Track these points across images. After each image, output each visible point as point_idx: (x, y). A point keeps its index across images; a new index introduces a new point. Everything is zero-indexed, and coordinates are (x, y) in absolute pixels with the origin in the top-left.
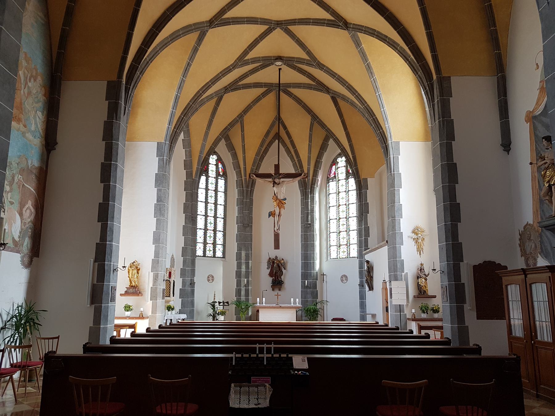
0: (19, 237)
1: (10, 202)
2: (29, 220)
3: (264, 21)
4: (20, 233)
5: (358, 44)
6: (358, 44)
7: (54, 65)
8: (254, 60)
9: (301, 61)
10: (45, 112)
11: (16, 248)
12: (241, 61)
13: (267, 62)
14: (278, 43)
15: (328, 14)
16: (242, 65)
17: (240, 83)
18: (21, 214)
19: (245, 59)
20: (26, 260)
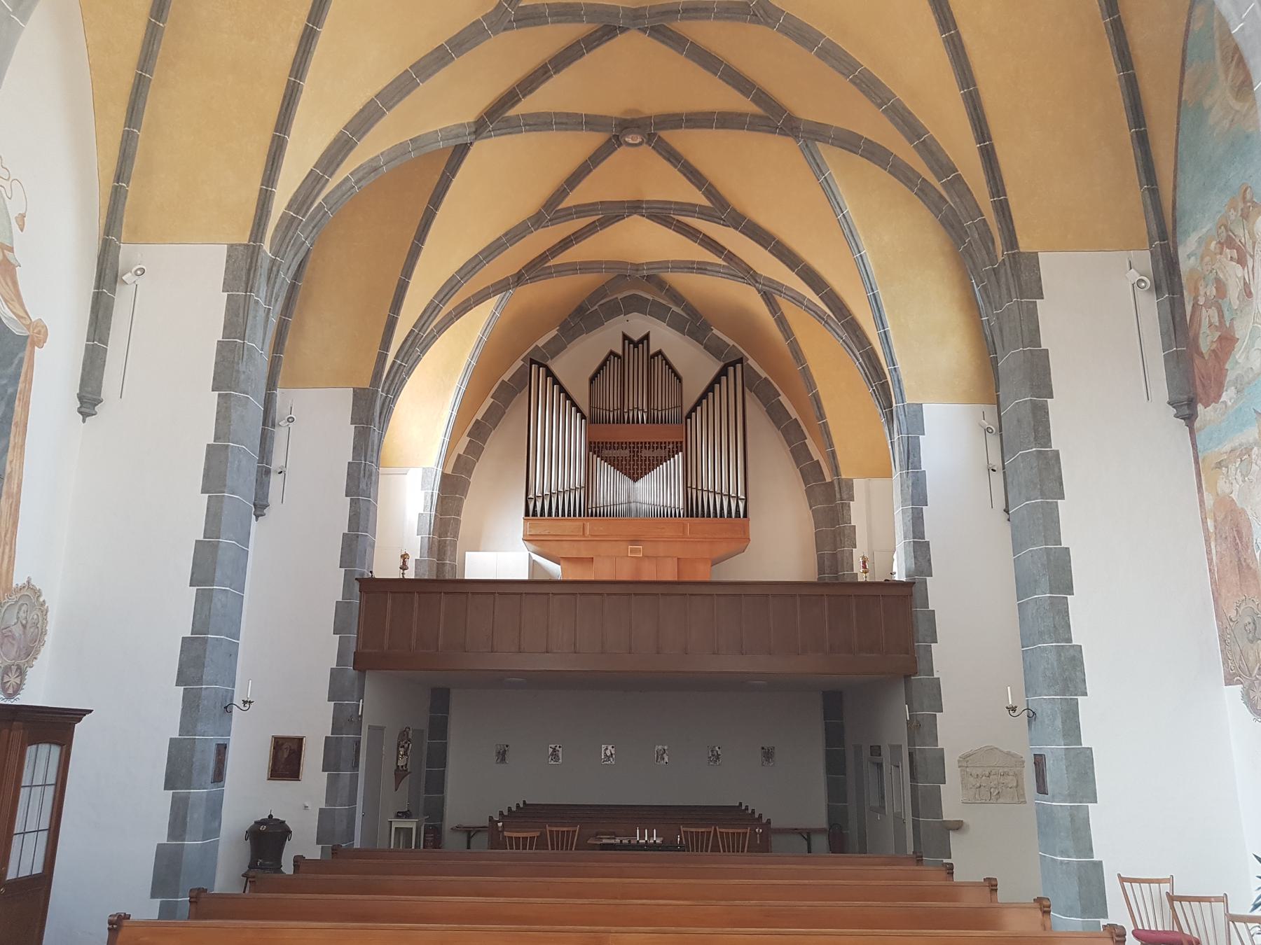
3: (591, 123)
5: (818, 168)
6: (818, 168)
7: (344, 171)
8: (581, 211)
9: (690, 209)
12: (550, 212)
13: (611, 213)
14: (639, 173)
15: (283, 209)
16: (553, 221)
17: (552, 262)
19: (560, 207)
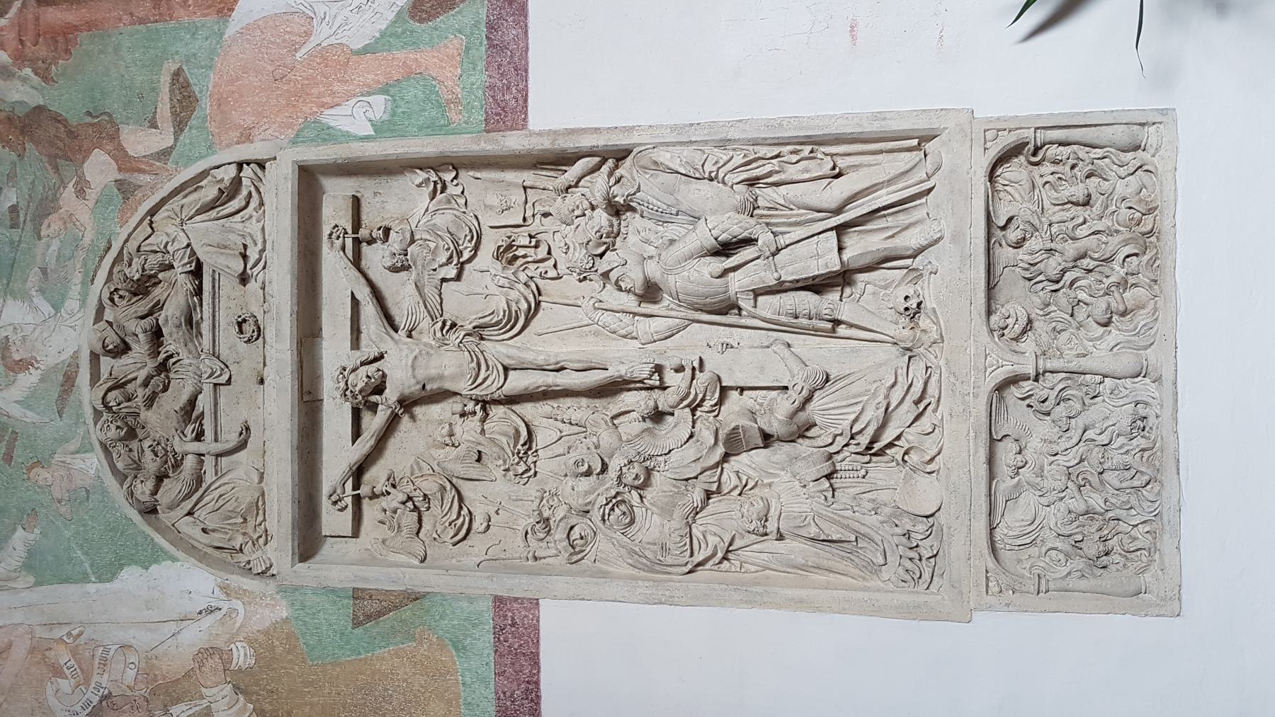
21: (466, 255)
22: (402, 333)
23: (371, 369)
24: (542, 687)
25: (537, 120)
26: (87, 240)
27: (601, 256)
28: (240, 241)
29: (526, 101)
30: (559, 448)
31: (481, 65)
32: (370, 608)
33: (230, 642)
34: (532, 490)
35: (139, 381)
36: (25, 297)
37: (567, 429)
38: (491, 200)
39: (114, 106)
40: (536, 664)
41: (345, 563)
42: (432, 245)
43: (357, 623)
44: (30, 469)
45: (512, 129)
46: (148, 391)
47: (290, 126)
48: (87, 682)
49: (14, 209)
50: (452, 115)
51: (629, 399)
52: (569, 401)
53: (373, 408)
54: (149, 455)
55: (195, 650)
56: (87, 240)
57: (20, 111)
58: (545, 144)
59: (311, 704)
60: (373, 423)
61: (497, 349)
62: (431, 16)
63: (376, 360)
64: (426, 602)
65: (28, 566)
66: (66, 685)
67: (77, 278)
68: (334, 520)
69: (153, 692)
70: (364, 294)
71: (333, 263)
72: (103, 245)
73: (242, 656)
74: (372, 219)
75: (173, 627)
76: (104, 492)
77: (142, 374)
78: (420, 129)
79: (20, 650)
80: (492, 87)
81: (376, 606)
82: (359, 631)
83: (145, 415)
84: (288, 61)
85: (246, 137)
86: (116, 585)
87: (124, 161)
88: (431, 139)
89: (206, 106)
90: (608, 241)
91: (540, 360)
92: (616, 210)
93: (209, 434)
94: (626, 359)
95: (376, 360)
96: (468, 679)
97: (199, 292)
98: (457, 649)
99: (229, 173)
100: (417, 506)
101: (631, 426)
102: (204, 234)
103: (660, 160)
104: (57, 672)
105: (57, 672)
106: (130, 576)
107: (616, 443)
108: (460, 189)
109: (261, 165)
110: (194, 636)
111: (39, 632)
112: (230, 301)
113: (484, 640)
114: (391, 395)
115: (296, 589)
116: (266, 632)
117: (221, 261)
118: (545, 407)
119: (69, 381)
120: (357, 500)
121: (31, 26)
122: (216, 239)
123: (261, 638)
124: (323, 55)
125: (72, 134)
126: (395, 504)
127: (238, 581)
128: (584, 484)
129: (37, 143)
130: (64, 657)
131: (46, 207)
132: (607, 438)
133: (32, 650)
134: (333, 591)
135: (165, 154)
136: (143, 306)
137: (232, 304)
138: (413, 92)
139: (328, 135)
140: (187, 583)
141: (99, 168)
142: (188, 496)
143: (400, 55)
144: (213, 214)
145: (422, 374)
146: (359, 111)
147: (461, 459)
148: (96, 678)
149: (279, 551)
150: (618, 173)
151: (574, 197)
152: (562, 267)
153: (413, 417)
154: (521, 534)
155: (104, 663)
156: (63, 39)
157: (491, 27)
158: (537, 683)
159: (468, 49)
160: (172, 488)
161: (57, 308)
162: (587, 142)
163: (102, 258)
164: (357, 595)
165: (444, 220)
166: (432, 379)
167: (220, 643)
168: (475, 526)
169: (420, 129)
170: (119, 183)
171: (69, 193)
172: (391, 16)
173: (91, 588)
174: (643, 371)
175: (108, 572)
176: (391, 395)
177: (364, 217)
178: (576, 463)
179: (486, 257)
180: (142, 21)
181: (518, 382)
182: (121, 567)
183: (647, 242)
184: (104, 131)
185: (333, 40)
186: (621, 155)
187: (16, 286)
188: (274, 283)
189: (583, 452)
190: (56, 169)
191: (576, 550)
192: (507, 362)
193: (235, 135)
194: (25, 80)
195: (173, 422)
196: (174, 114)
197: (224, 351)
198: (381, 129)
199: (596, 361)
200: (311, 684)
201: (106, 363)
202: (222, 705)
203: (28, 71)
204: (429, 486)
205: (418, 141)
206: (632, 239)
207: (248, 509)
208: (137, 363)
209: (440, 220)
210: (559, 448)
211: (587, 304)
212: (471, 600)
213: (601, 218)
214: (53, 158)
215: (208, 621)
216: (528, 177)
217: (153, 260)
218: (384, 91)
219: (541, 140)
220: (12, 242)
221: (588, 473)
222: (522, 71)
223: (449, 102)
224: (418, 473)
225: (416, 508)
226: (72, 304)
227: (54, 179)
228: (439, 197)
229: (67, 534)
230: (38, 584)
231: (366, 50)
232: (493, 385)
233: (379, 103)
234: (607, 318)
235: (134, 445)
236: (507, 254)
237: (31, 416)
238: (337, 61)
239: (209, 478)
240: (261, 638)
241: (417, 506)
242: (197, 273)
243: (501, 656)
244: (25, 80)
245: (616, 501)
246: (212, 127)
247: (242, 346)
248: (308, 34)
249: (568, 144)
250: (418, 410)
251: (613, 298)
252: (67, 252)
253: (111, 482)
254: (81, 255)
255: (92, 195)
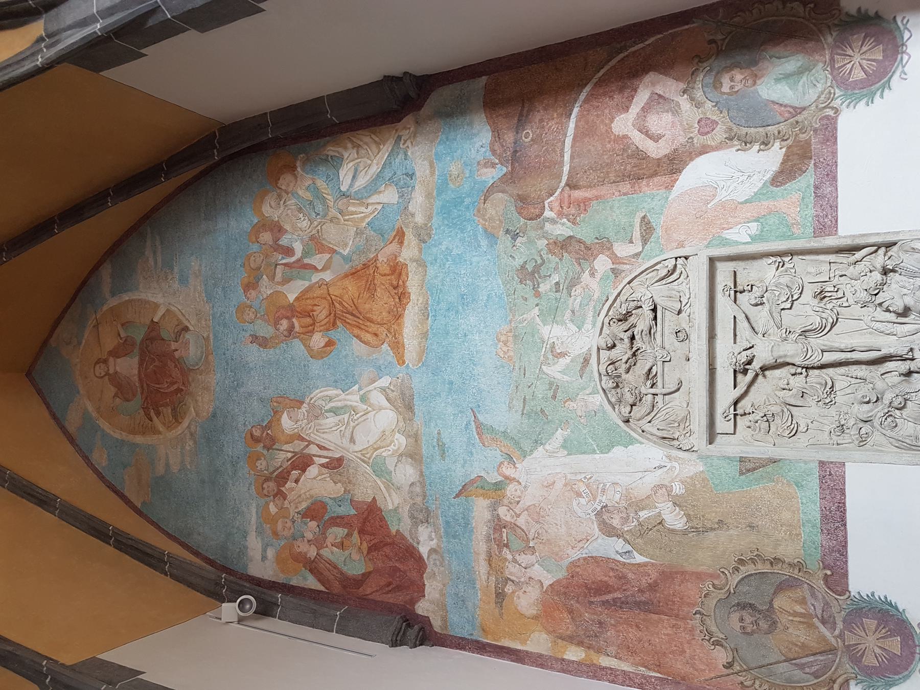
0: (766, 143)
1: (645, 241)
2: (684, 103)
4: (746, 142)
10: (331, 150)
11: (808, 153)
18: (673, 164)
20: (859, 59)
21: (795, 297)
22: (760, 335)
23: (749, 352)
24: (847, 505)
25: (841, 232)
26: (596, 297)
27: (876, 295)
28: (678, 295)
29: (837, 221)
30: (849, 391)
31: (811, 206)
32: (748, 466)
33: (672, 481)
34: (833, 411)
35: (624, 361)
36: (563, 323)
37: (854, 381)
38: (810, 271)
39: (611, 234)
40: (843, 492)
41: (732, 446)
42: (777, 293)
43: (741, 473)
44: (565, 403)
45: (829, 235)
46: (628, 365)
47: (705, 239)
48: (595, 499)
49: (557, 284)
50: (795, 230)
51: (890, 365)
52: (855, 367)
53: (745, 372)
54: (628, 394)
55: (652, 486)
56: (596, 297)
57: (560, 239)
58: (849, 242)
59: (716, 512)
60: (744, 381)
61: (816, 342)
62: (782, 184)
63: (750, 348)
64: (781, 464)
65: (564, 447)
66: (583, 501)
67: (591, 314)
68: (722, 425)
69: (630, 505)
70: (741, 318)
71: (723, 303)
72: (605, 298)
73: (678, 489)
74: (742, 283)
75: (640, 475)
76: (604, 412)
77: (625, 358)
78: (777, 237)
79: (559, 485)
80: (817, 216)
81: (752, 465)
82: (743, 477)
83: (624, 376)
84: (704, 208)
85: (681, 245)
86: (610, 455)
87: (615, 259)
88: (781, 243)
89: (659, 232)
90: (880, 288)
91: (842, 346)
92: (885, 272)
93: (659, 384)
94: (890, 346)
95: (750, 348)
96: (804, 501)
97: (655, 318)
98: (798, 486)
99: (671, 264)
100: (768, 419)
101: (894, 379)
102: (659, 293)
103: (916, 247)
104: (579, 495)
105: (579, 495)
106: (618, 451)
107: (886, 387)
108: (792, 266)
109: (686, 258)
110: (652, 479)
111: (569, 476)
112: (668, 322)
113: (814, 483)
114: (756, 365)
115: (708, 457)
116: (691, 478)
117: (669, 304)
118: (842, 370)
119: (586, 361)
120: (735, 415)
121: (566, 200)
122: (666, 293)
123: (688, 480)
124: (723, 205)
125: (588, 248)
126: (758, 418)
127: (675, 453)
128: (866, 407)
129: (569, 253)
130: (582, 488)
131: (573, 283)
132: (880, 385)
133: (565, 485)
134: (729, 458)
135: (637, 255)
136: (625, 326)
137: (672, 324)
138: (773, 220)
139: (725, 242)
140: (648, 454)
141: (602, 263)
142: (649, 414)
143: (765, 203)
144: (664, 282)
145: (776, 354)
146: (743, 231)
147: (794, 396)
148: (599, 498)
149: (698, 438)
150: (889, 254)
151: (861, 267)
152: (851, 301)
153: (764, 376)
154: (827, 433)
155: (603, 491)
156: (583, 205)
157: (816, 187)
158: (844, 503)
159: (803, 198)
160: (638, 411)
161: (580, 328)
162: (872, 240)
163: (604, 305)
164: (742, 460)
165: (785, 280)
166: (780, 357)
167: (666, 483)
168: (800, 429)
169: (777, 237)
170: (613, 270)
171: (586, 275)
172: (760, 185)
173: (597, 456)
174: (902, 351)
175: (607, 448)
176: (756, 365)
177: (738, 280)
178: (863, 397)
179: (808, 296)
180: (625, 194)
181: (829, 358)
182: (613, 447)
183: (904, 287)
184: (605, 245)
185: (728, 198)
186: (889, 245)
187: (558, 319)
188: (696, 314)
189: (864, 391)
190: (580, 264)
191: (862, 441)
192: (823, 348)
193: (675, 245)
194: (563, 224)
195: (643, 378)
196: (642, 236)
197: (667, 346)
198: (754, 239)
199: (876, 346)
200: (716, 502)
201: (604, 354)
202: (667, 511)
203: (565, 220)
204: (776, 409)
205: (776, 243)
206: (894, 286)
207: (682, 420)
208: (622, 352)
209: (782, 280)
210: (849, 391)
211: (867, 319)
212: (806, 463)
213: (877, 276)
214: (578, 260)
215: (660, 471)
216: (832, 258)
217: (633, 304)
218: (757, 220)
219: (845, 240)
220: (556, 299)
221: (868, 402)
222: (834, 207)
223: (793, 224)
224: (767, 403)
225: (768, 421)
226: (588, 326)
227: (578, 269)
228: (780, 269)
229: (584, 432)
230: (568, 454)
231: (746, 202)
232: (815, 360)
233: (754, 227)
234: (878, 325)
235: (619, 390)
236: (821, 295)
237: (566, 378)
238: (731, 209)
239: (660, 405)
240: (688, 480)
241: (768, 419)
242: (654, 310)
243: (824, 490)
244: (563, 224)
245: (888, 415)
246: (662, 241)
247: (677, 344)
248: (714, 196)
249: (862, 242)
250: (767, 373)
251: (880, 314)
252: (585, 302)
253: (608, 408)
254: (592, 304)
255: (598, 276)
